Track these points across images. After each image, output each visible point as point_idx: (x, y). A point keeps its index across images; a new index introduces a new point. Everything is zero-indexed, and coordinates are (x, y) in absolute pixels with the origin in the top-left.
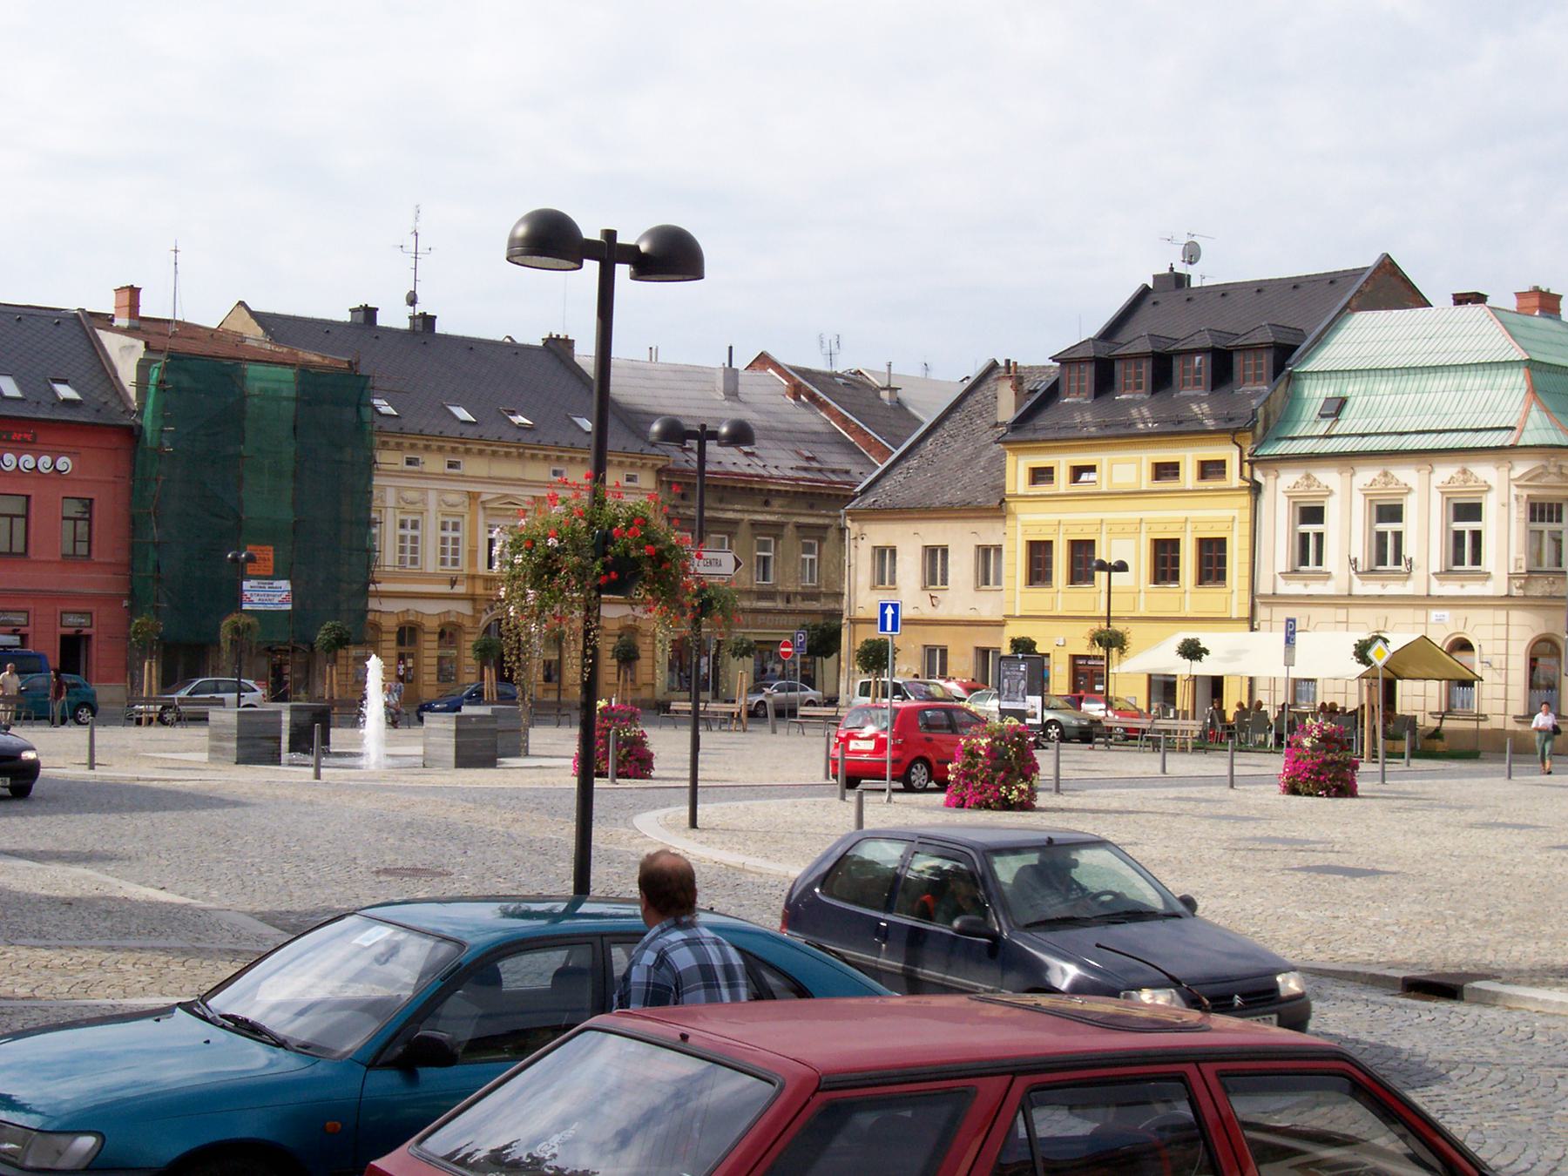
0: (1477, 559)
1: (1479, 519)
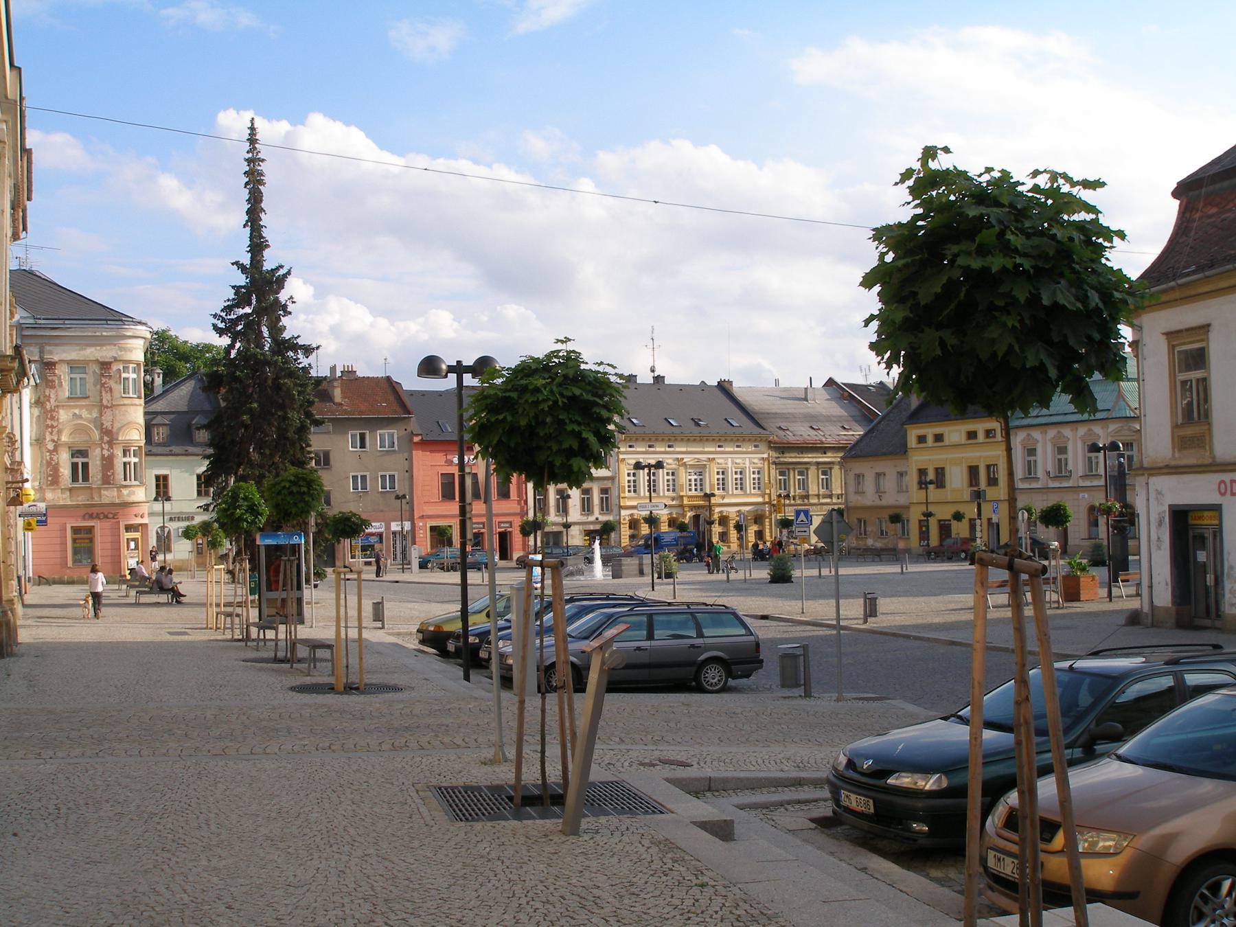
0: (86, 478)
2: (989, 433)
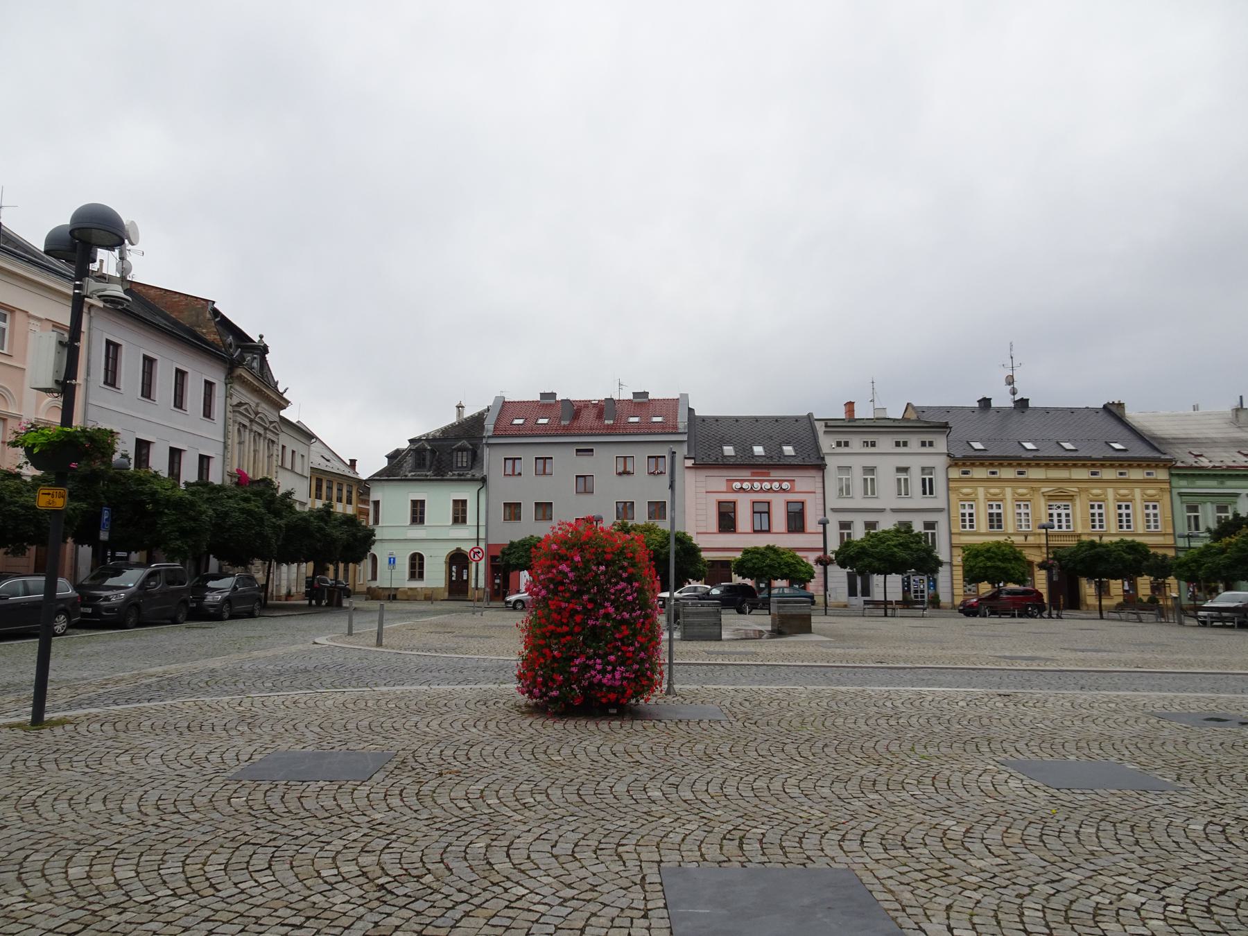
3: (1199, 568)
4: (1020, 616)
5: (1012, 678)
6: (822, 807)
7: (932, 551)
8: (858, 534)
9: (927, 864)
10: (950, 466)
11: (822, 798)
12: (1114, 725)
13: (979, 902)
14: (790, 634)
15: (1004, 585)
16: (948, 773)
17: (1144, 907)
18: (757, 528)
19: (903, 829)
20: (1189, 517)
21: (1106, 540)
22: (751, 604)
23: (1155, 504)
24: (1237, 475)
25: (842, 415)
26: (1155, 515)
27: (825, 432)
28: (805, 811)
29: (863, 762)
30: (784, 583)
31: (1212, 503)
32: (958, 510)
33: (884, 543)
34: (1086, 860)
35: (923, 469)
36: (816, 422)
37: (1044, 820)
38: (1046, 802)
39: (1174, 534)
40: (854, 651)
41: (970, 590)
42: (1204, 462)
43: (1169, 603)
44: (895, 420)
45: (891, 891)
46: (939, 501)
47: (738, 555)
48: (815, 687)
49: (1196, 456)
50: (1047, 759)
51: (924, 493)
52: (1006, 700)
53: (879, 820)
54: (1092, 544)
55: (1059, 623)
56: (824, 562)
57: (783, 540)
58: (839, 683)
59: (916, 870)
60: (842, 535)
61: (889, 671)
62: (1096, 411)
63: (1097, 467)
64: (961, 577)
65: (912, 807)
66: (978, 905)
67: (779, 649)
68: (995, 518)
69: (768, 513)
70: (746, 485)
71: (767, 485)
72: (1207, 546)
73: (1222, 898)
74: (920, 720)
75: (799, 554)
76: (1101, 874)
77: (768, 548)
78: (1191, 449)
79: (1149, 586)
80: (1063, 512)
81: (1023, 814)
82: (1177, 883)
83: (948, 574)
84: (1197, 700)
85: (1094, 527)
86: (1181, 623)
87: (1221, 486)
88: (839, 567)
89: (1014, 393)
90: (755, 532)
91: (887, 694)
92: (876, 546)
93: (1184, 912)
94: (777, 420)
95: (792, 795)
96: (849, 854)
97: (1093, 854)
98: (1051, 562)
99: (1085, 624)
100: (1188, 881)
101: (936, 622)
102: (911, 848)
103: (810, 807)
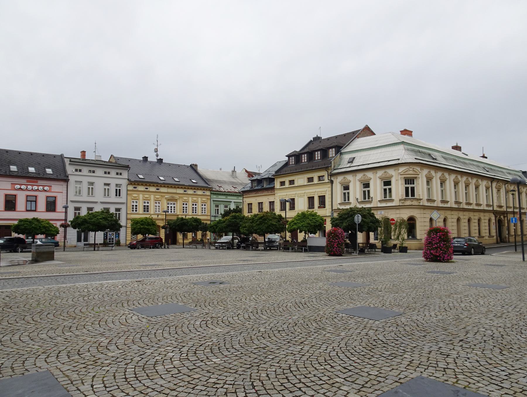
1: (391, 185)
2: (320, 178)
3: (217, 228)
4: (153, 248)
5: (144, 274)
6: (40, 344)
7: (118, 221)
8: (84, 212)
9: (88, 360)
10: (129, 184)
11: (41, 339)
12: (178, 289)
13: (108, 371)
14: (42, 261)
15: (148, 236)
16: (107, 317)
17: (174, 357)
18: (29, 208)
19: (80, 346)
20: (216, 209)
21: (187, 217)
22: (22, 247)
23: (136, 201)
24: (225, 194)
25: (79, 156)
26: (205, 208)
27: (70, 164)
28: (30, 347)
29: (67, 319)
30: (42, 236)
31: (223, 204)
32: (131, 203)
33: (96, 217)
34: (156, 343)
35: (117, 185)
36: (65, 159)
37: (143, 331)
38: (146, 323)
39: (210, 215)
40: (75, 267)
41: (134, 238)
42: (222, 189)
43: (207, 241)
44: (105, 162)
45: (67, 376)
46: (123, 199)
47: (16, 223)
48: (49, 286)
49: (219, 187)
50: (150, 305)
51: (116, 195)
52: (139, 283)
53: (69, 344)
54: (182, 219)
55: (168, 250)
56: (65, 226)
57: (42, 214)
58: (63, 283)
59: (82, 364)
60: (75, 213)
61: (90, 275)
62: (188, 167)
63: (186, 189)
64: (130, 232)
65: (87, 335)
66: (108, 372)
67: (33, 269)
68: (146, 207)
69: (36, 201)
70: (23, 187)
71: (36, 188)
72: (220, 220)
73: (201, 347)
74: (99, 296)
75: (51, 222)
76: (160, 348)
77: (34, 219)
78: (218, 184)
79: (201, 235)
80: (173, 206)
81: (135, 330)
82: (187, 345)
83: (125, 231)
84: (207, 276)
85: (183, 212)
86: (210, 248)
87: (226, 198)
88: (72, 228)
89: (157, 156)
90: (27, 211)
91: (86, 286)
92: (92, 219)
93: (187, 355)
94: (43, 155)
95: (23, 341)
96: (49, 363)
97: (159, 341)
98: (166, 226)
99: (177, 250)
100: (190, 344)
101: (117, 252)
102: (82, 354)
103: (33, 345)
